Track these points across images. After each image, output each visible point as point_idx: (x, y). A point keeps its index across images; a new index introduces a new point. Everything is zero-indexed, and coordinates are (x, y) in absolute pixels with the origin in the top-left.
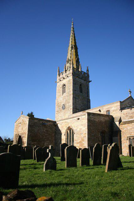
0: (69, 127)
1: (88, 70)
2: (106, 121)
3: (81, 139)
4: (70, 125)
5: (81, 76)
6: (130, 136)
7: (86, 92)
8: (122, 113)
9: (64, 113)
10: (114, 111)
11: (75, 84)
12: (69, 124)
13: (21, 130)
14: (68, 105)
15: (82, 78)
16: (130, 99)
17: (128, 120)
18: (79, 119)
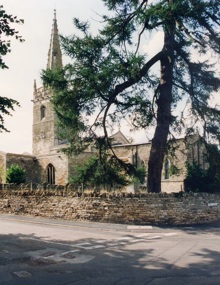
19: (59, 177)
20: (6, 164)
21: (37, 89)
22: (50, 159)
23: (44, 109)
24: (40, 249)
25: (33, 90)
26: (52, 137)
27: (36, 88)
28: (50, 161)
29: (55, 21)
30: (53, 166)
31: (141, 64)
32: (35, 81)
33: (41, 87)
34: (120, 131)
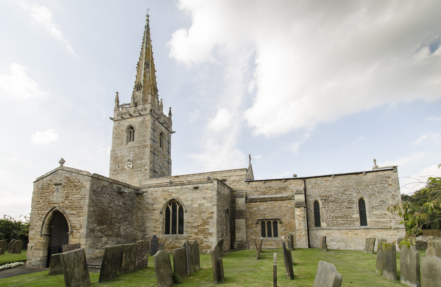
1: (170, 114)
3: (202, 221)
4: (174, 196)
6: (263, 218)
8: (249, 186)
12: (173, 195)
14: (139, 162)
15: (162, 124)
17: (258, 197)
18: (196, 188)
20: (90, 196)
21: (120, 104)
25: (114, 105)
26: (146, 167)
27: (118, 104)
28: (173, 195)
29: (147, 27)
30: (179, 204)
32: (170, 109)
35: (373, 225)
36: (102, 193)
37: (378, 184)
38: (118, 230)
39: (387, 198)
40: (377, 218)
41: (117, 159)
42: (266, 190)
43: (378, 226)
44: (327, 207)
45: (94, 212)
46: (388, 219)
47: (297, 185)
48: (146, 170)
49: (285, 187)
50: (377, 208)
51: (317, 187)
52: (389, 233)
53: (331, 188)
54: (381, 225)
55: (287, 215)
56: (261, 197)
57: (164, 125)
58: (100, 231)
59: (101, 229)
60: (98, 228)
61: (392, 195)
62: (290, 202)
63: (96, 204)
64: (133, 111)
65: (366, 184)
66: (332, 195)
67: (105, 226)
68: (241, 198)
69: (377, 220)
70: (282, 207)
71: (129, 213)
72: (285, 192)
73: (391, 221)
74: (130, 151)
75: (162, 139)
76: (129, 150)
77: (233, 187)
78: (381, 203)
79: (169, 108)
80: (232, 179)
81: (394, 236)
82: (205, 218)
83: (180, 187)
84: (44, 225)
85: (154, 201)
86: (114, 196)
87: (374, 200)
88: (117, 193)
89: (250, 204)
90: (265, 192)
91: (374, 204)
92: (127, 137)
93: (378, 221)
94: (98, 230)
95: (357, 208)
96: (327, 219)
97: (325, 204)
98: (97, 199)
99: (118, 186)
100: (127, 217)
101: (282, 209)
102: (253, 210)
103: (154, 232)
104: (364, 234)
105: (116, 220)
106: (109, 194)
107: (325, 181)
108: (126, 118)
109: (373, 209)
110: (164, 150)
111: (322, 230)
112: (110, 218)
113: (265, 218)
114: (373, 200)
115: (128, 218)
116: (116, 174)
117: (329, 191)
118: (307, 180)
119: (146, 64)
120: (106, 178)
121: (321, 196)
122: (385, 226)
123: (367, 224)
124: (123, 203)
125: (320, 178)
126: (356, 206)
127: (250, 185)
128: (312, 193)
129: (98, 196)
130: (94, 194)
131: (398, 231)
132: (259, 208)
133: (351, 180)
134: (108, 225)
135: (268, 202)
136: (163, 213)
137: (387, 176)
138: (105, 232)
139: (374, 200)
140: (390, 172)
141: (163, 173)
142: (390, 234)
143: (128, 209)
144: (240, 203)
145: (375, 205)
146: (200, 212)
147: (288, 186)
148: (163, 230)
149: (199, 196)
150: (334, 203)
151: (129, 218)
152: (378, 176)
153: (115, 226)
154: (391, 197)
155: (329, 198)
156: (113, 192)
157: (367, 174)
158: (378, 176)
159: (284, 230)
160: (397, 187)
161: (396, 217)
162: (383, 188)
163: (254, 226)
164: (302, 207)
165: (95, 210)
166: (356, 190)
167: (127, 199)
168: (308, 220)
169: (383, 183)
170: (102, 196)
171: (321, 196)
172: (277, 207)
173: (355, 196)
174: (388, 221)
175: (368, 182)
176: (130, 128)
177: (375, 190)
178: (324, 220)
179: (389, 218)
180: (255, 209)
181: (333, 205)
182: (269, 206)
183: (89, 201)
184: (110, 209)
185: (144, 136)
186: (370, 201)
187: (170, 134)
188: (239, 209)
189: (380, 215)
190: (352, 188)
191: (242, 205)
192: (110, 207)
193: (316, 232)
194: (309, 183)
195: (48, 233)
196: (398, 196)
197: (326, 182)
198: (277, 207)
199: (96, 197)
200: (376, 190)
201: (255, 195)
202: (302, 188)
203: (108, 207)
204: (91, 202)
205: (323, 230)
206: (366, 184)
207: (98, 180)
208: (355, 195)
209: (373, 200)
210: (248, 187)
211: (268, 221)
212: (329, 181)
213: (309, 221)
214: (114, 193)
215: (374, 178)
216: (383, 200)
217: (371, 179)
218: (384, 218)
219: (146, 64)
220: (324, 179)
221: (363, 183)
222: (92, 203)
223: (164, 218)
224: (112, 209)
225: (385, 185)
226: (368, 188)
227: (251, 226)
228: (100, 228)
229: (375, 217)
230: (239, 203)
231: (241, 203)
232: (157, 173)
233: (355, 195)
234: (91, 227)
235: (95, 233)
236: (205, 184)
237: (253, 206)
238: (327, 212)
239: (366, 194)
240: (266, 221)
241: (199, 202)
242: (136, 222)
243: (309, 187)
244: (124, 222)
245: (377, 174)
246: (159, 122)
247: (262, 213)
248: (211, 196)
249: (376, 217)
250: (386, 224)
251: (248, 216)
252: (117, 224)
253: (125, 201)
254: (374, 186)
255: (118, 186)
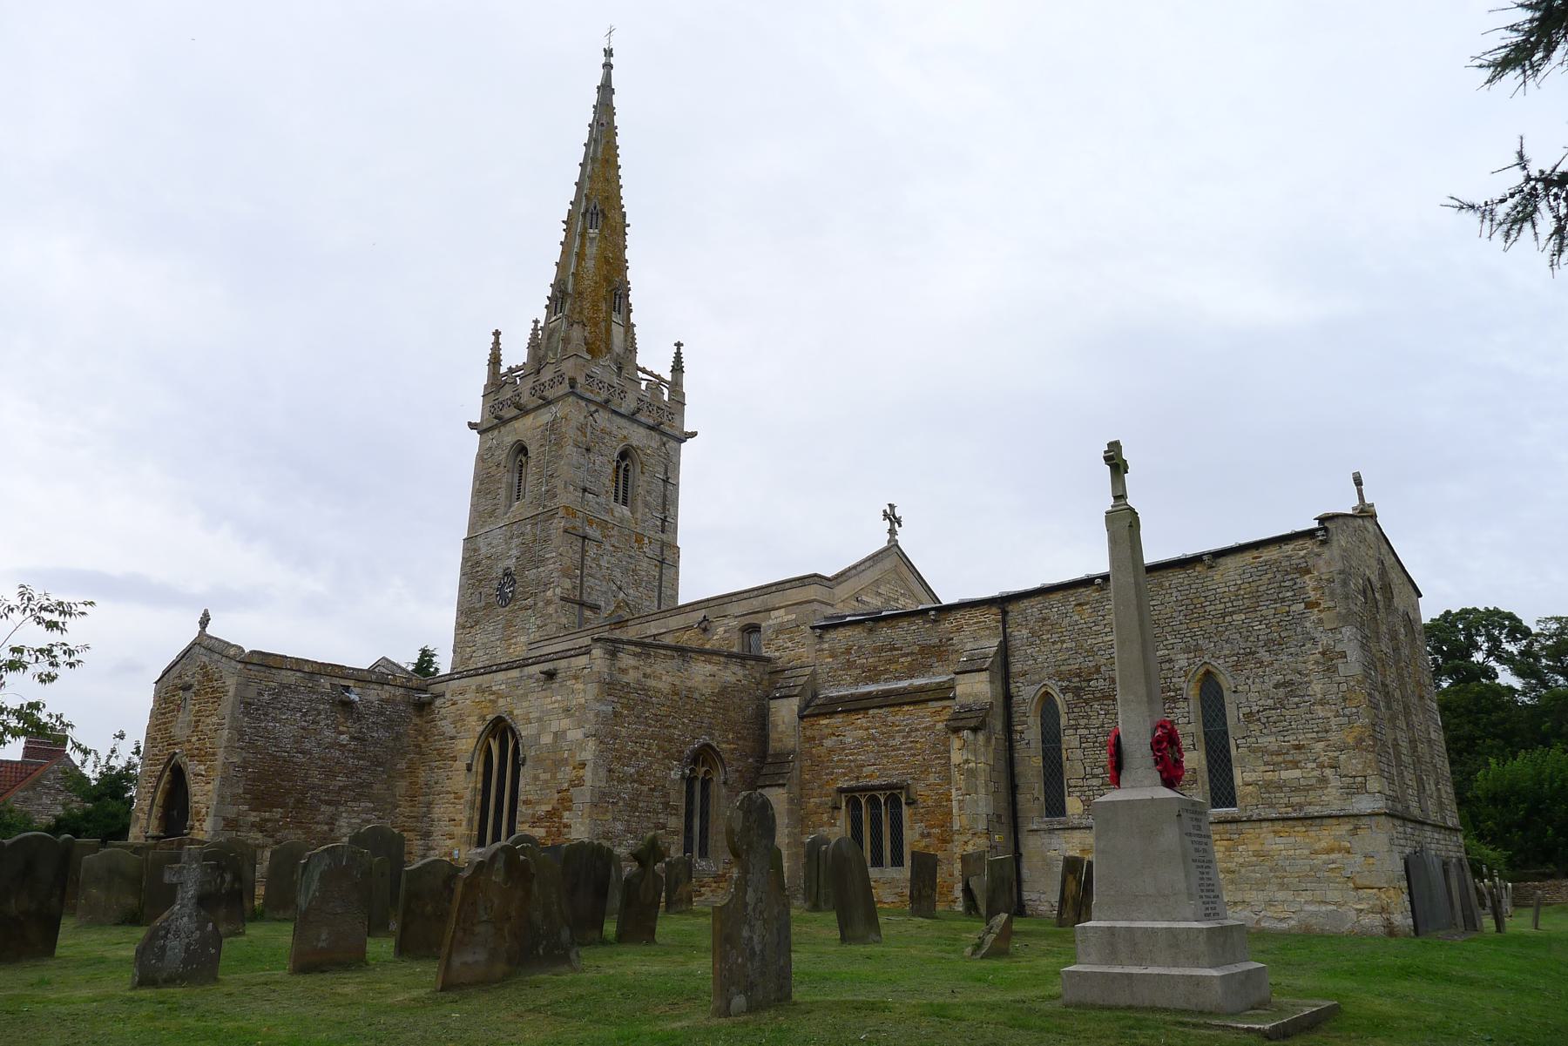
0: (499, 720)
1: (678, 367)
2: (724, 691)
3: (556, 796)
5: (628, 405)
6: (853, 783)
7: (655, 500)
8: (826, 646)
9: (509, 624)
10: (780, 630)
11: (588, 450)
12: (501, 702)
13: (188, 732)
15: (631, 417)
16: (888, 564)
19: (538, 803)
22: (499, 695)
23: (524, 460)
24: (1130, 537)
28: (501, 702)
29: (606, 89)
31: (670, 379)
32: (679, 349)
33: (649, 369)
34: (893, 549)
35: (1255, 802)
36: (274, 708)
37: (1267, 603)
38: (326, 828)
39: (1300, 667)
40: (1267, 768)
41: (477, 569)
42: (877, 659)
43: (1274, 808)
44: (1083, 722)
45: (245, 768)
46: (1309, 772)
47: (982, 633)
48: (548, 603)
49: (940, 641)
50: (1265, 720)
51: (1049, 636)
52: (1320, 840)
53: (1097, 634)
54: (1286, 800)
55: (931, 766)
56: (861, 691)
57: (642, 417)
58: (260, 827)
59: (262, 820)
60: (253, 817)
61: (1323, 654)
62: (945, 708)
63: (251, 742)
64: (529, 391)
65: (1222, 606)
66: (1100, 667)
67: (278, 813)
68: (785, 701)
69: (1269, 776)
70: (917, 730)
71: (376, 770)
72: (943, 666)
73: (1323, 780)
74: (511, 538)
75: (634, 470)
76: (508, 534)
77: (777, 654)
78: (1281, 692)
79: (675, 345)
80: (775, 622)
81: (1340, 855)
82: (566, 786)
83: (515, 673)
84: (155, 807)
85: (455, 727)
86: (319, 714)
87: (1251, 680)
88: (333, 704)
89: (813, 725)
90: (875, 668)
91: (1255, 701)
92: (511, 485)
93: (1271, 781)
94: (253, 825)
95: (1189, 723)
96: (1083, 779)
97: (1075, 710)
98: (255, 728)
99: (336, 681)
100: (370, 785)
101: (917, 742)
102: (823, 750)
103: (450, 839)
104: (1223, 849)
105: (322, 792)
106: (301, 711)
107: (1076, 605)
108: (511, 419)
109: (1252, 727)
110: (639, 515)
111: (1067, 832)
112: (300, 786)
113: (863, 782)
114: (1250, 682)
115: (371, 788)
116: (472, 627)
117: (1091, 652)
118: (1014, 609)
119: (588, 215)
120: (291, 662)
121: (1060, 676)
122: (1301, 806)
123: (1234, 798)
124: (353, 738)
125: (1059, 596)
126: (1189, 712)
127: (827, 642)
128: (1029, 663)
129: (262, 717)
130: (247, 714)
131: (1356, 828)
132: (841, 738)
133: (1167, 596)
134: (290, 810)
135: (871, 712)
136: (474, 769)
137: (1297, 565)
138: (278, 831)
139: (1251, 680)
140: (1309, 544)
141: (628, 605)
142: (1323, 844)
143: (375, 756)
144: (784, 723)
145: (1260, 703)
146: (554, 762)
147: (951, 636)
148: (472, 830)
149: (556, 705)
150: (1109, 706)
151: (378, 788)
152: (1265, 568)
153: (317, 813)
154: (1317, 663)
155: (1092, 680)
156: (318, 701)
157: (1222, 560)
158: (1265, 568)
159: (923, 836)
160: (1339, 613)
161: (1342, 757)
162: (1285, 623)
163: (825, 817)
164: (964, 728)
165: (245, 763)
166: (1185, 640)
167: (373, 723)
168: (1017, 786)
169: (1283, 600)
170: (274, 719)
171: (1060, 676)
172: (899, 731)
173: (1181, 669)
174: (1314, 781)
175: (1227, 600)
176: (520, 452)
177: (1254, 633)
178: (1075, 787)
179: (1314, 765)
180: (828, 743)
181: (1106, 714)
182: (874, 731)
183: (229, 733)
184: (300, 758)
185: (551, 476)
186: (1240, 688)
187: (672, 444)
188: (780, 744)
189: (1278, 754)
190: (1170, 629)
191: (787, 728)
192: (300, 753)
193: (1046, 839)
194: (1020, 619)
195: (161, 831)
196: (1346, 657)
197: (1079, 608)
198: (899, 731)
199: (251, 721)
200: (1258, 633)
201: (844, 682)
202: (992, 644)
203: (295, 750)
204: (236, 737)
205: (1070, 831)
206: (1222, 606)
207: (263, 669)
208: (1182, 661)
209: (1250, 682)
210: (823, 650)
211: (869, 793)
212: (1087, 604)
213: (1021, 791)
214: (322, 707)
215: (1251, 580)
216: (1288, 678)
217: (1239, 582)
218: (1296, 765)
219: (588, 215)
220: (1071, 599)
221: (1208, 603)
222: (239, 740)
223: (476, 788)
224: (309, 758)
225: (1293, 608)
226: (1230, 627)
227: (815, 818)
228: (258, 819)
229: (1260, 762)
230: (780, 722)
231: (786, 720)
232: (595, 608)
233: (1182, 661)
234: (231, 812)
235: (239, 834)
236: (574, 659)
237: (822, 733)
238: (1084, 749)
239: (1222, 653)
240: (865, 796)
241: (555, 727)
242: (410, 804)
243: (1020, 634)
244: (354, 800)
245: (1261, 557)
246: (614, 412)
247: (850, 761)
248: (583, 701)
249: (1266, 764)
250: (1305, 793)
251: (807, 777)
252: (323, 808)
253: (364, 730)
254: (1253, 615)
255: (336, 681)
